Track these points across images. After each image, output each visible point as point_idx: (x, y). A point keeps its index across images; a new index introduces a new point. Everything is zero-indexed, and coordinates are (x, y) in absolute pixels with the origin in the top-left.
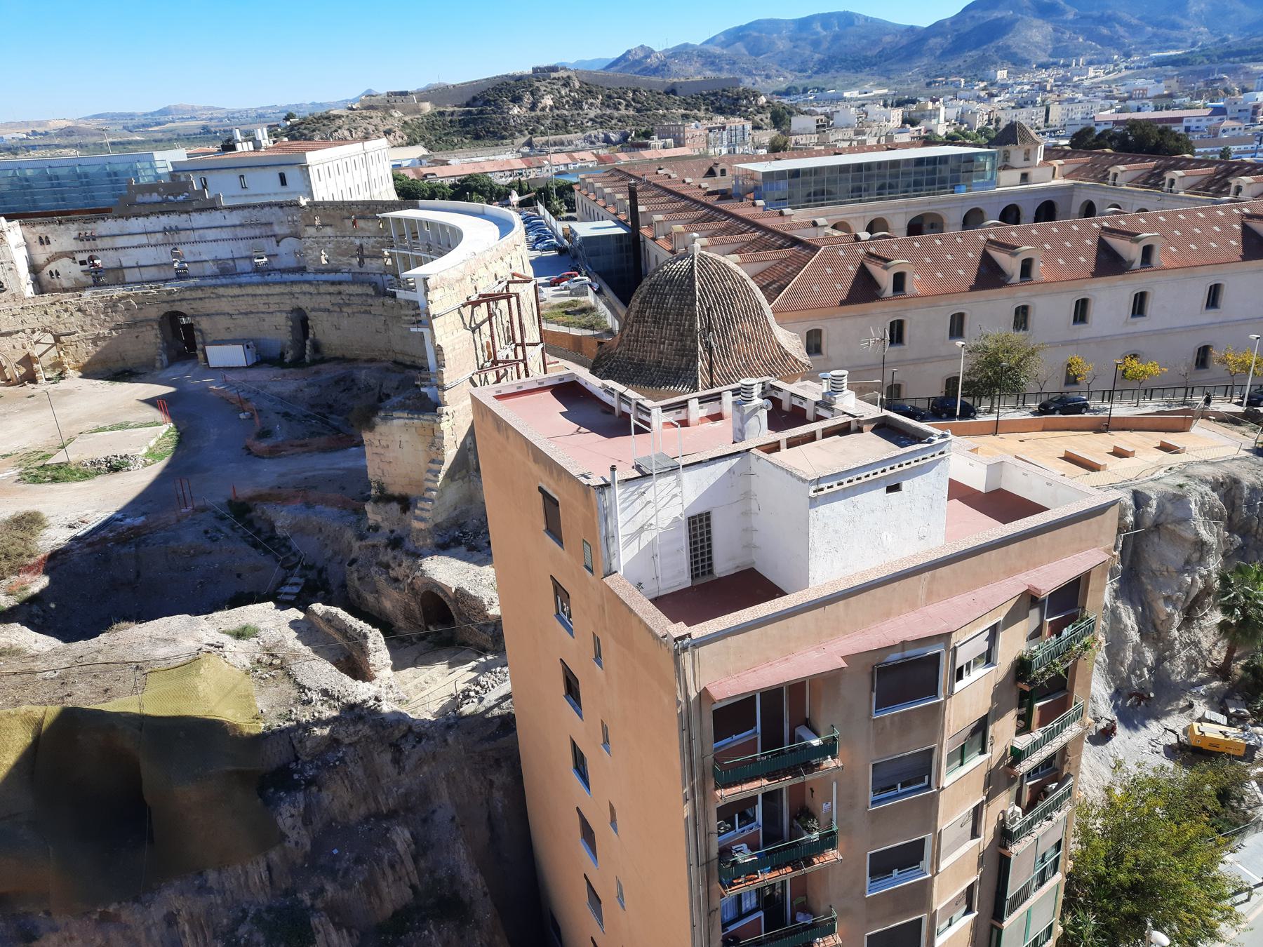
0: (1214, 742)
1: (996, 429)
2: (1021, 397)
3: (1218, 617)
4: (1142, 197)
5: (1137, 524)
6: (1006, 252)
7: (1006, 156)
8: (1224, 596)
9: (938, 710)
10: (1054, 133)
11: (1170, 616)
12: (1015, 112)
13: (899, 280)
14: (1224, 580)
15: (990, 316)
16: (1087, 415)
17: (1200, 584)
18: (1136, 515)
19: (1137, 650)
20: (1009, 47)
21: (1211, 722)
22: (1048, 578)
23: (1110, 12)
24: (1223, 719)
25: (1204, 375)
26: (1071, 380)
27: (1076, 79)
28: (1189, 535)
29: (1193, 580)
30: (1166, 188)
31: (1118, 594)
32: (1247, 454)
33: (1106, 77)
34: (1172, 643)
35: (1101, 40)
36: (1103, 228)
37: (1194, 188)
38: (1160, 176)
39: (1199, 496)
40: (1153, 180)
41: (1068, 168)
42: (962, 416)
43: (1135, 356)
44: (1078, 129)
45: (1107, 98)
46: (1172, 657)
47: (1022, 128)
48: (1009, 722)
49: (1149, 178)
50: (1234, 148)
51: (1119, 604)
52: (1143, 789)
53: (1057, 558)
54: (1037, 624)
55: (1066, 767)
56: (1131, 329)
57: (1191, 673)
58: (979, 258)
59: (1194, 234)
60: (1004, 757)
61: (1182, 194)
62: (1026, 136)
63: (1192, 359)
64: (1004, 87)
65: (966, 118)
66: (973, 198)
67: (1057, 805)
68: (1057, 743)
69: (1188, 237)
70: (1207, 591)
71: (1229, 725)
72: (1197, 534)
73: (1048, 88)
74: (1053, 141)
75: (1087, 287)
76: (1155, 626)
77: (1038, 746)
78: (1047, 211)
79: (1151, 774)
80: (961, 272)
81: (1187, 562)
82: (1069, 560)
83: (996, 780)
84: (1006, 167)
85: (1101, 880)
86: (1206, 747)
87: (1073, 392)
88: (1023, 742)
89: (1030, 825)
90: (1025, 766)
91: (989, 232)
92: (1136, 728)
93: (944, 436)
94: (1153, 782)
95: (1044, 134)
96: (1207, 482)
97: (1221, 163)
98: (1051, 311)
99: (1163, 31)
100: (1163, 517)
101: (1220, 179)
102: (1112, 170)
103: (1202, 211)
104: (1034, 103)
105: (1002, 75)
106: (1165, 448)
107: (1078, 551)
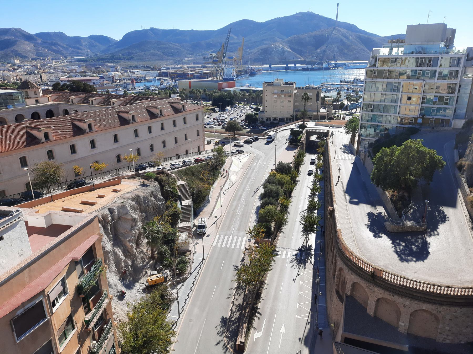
0: (156, 281)
1: (52, 199)
2: (59, 185)
3: (146, 241)
4: (82, 108)
5: (113, 219)
6: (35, 130)
7: (27, 94)
8: (146, 233)
9: (48, 324)
10: (46, 84)
11: (132, 246)
12: (27, 76)
13: (46, 136)
14: (144, 228)
15: (37, 156)
16: (86, 186)
17: (138, 232)
18: (111, 216)
19: (125, 262)
20: (17, 51)
21: (153, 275)
22: (79, 252)
23: (54, 41)
24: (156, 272)
25: (120, 164)
26: (77, 175)
27: (49, 65)
28: (130, 218)
29: (135, 232)
30: (91, 103)
31: (114, 245)
32: (139, 187)
33: (60, 65)
34: (135, 255)
35: (54, 51)
36: (27, 126)
37: (100, 103)
38: (88, 99)
39: (129, 204)
40: (86, 101)
41: (54, 98)
42: (36, 198)
43: (97, 162)
44: (54, 83)
45: (62, 72)
46: (136, 259)
47: (30, 83)
48: (81, 311)
49: (84, 100)
50: (110, 90)
51: (115, 248)
52: (138, 308)
53: (80, 244)
54: (81, 270)
55: (108, 317)
56: (93, 153)
57: (143, 262)
58: (25, 134)
59: (103, 119)
60: (83, 326)
61: (97, 105)
62: (33, 86)
63: (115, 160)
64: (20, 67)
65: (5, 78)
66: (18, 110)
67: (108, 332)
68: (101, 310)
69: (102, 120)
70: (140, 234)
71: (158, 273)
72: (132, 217)
73: (39, 67)
74: (46, 87)
75: (72, 140)
76: (128, 252)
77: (93, 316)
78: (50, 114)
79: (139, 302)
80: (19, 140)
81: (132, 227)
82: (85, 243)
83: (81, 338)
84: (28, 98)
85: (133, 347)
86: (154, 284)
87: (79, 179)
88: (88, 317)
89: (101, 346)
90: (92, 325)
91: (27, 123)
92: (132, 288)
93: (18, 211)
94: (141, 304)
95: (42, 85)
96: (130, 199)
97: (106, 95)
98: (62, 151)
99: (75, 50)
100: (120, 214)
101: (107, 99)
102: (70, 98)
103: (104, 111)
104: (34, 73)
105: (17, 61)
106: (115, 191)
107: (88, 238)
